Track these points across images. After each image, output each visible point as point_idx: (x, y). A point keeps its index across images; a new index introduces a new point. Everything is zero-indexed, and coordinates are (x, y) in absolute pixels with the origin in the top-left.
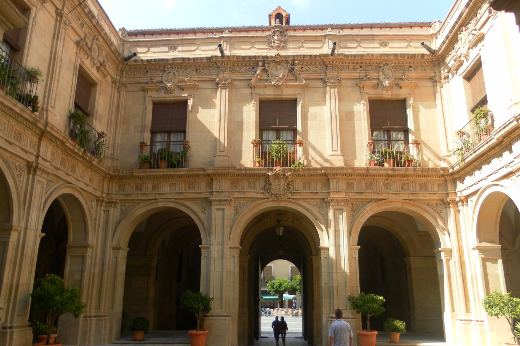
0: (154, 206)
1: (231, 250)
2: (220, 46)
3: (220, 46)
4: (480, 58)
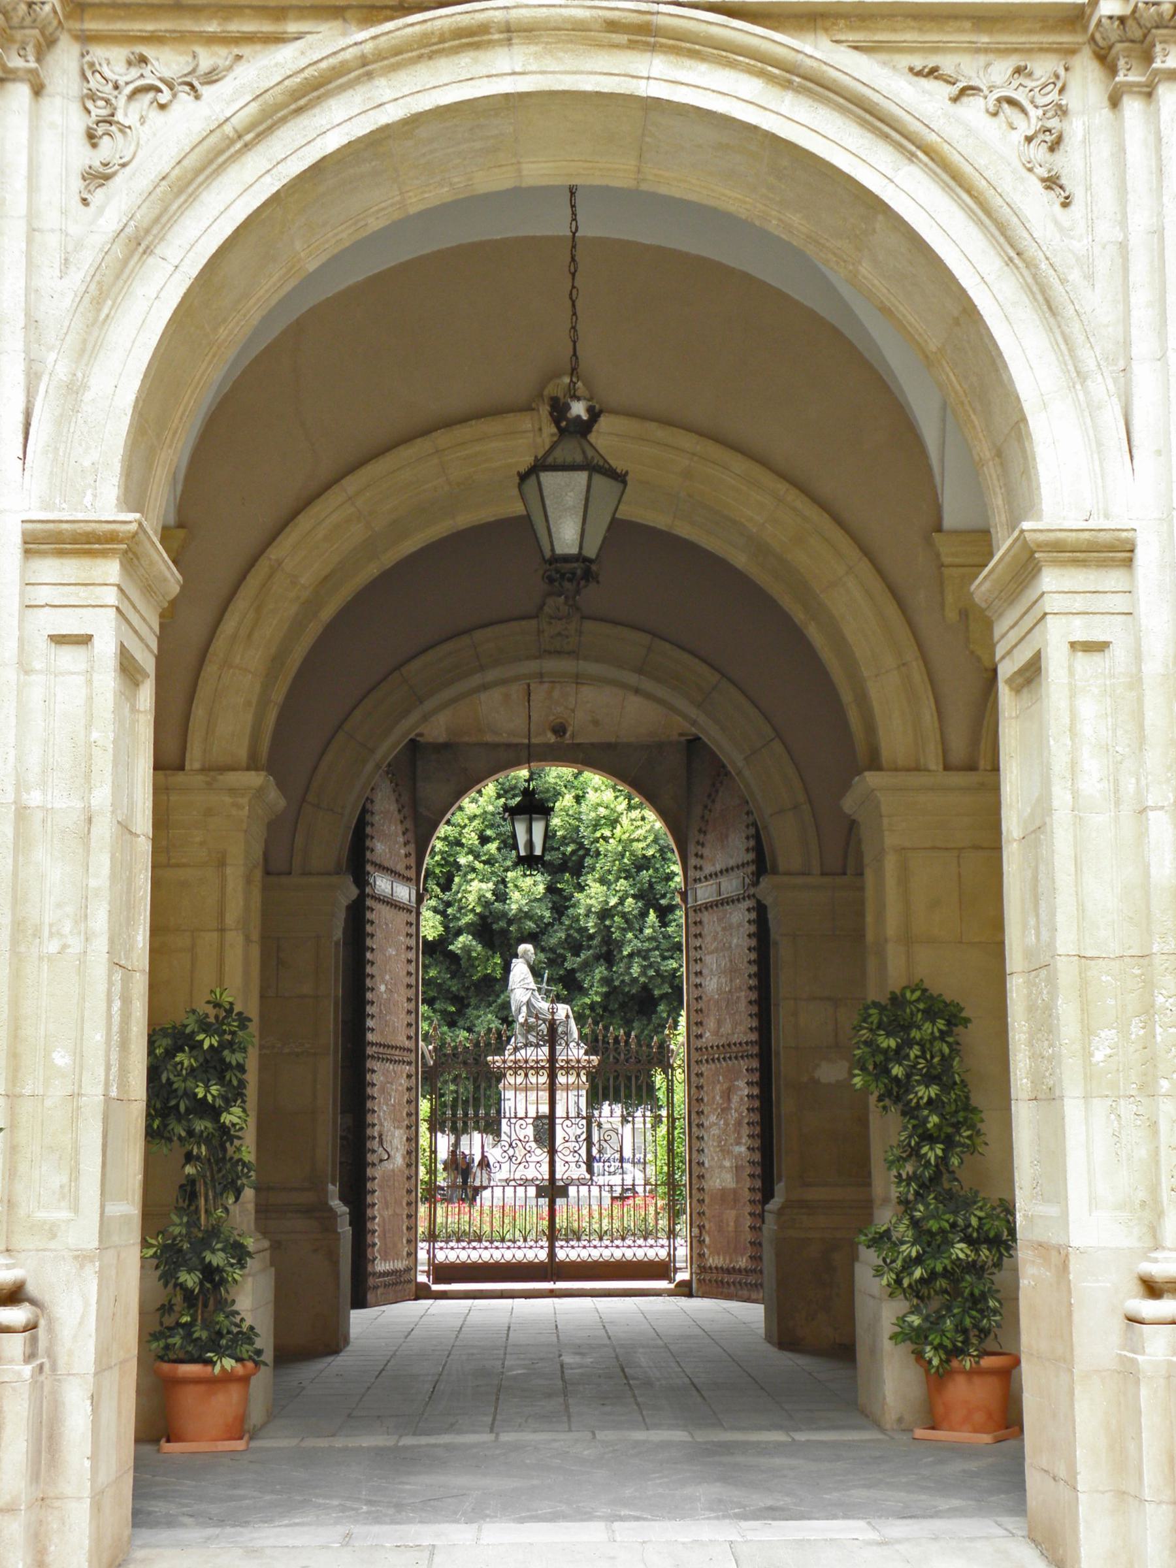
1: (49, 569)
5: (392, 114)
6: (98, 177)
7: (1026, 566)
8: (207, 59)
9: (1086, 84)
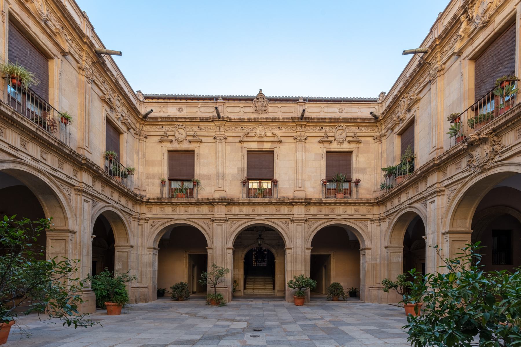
0: (172, 223)
2: (216, 108)
3: (216, 108)
4: (414, 118)
5: (12, 168)
9: (290, 222)
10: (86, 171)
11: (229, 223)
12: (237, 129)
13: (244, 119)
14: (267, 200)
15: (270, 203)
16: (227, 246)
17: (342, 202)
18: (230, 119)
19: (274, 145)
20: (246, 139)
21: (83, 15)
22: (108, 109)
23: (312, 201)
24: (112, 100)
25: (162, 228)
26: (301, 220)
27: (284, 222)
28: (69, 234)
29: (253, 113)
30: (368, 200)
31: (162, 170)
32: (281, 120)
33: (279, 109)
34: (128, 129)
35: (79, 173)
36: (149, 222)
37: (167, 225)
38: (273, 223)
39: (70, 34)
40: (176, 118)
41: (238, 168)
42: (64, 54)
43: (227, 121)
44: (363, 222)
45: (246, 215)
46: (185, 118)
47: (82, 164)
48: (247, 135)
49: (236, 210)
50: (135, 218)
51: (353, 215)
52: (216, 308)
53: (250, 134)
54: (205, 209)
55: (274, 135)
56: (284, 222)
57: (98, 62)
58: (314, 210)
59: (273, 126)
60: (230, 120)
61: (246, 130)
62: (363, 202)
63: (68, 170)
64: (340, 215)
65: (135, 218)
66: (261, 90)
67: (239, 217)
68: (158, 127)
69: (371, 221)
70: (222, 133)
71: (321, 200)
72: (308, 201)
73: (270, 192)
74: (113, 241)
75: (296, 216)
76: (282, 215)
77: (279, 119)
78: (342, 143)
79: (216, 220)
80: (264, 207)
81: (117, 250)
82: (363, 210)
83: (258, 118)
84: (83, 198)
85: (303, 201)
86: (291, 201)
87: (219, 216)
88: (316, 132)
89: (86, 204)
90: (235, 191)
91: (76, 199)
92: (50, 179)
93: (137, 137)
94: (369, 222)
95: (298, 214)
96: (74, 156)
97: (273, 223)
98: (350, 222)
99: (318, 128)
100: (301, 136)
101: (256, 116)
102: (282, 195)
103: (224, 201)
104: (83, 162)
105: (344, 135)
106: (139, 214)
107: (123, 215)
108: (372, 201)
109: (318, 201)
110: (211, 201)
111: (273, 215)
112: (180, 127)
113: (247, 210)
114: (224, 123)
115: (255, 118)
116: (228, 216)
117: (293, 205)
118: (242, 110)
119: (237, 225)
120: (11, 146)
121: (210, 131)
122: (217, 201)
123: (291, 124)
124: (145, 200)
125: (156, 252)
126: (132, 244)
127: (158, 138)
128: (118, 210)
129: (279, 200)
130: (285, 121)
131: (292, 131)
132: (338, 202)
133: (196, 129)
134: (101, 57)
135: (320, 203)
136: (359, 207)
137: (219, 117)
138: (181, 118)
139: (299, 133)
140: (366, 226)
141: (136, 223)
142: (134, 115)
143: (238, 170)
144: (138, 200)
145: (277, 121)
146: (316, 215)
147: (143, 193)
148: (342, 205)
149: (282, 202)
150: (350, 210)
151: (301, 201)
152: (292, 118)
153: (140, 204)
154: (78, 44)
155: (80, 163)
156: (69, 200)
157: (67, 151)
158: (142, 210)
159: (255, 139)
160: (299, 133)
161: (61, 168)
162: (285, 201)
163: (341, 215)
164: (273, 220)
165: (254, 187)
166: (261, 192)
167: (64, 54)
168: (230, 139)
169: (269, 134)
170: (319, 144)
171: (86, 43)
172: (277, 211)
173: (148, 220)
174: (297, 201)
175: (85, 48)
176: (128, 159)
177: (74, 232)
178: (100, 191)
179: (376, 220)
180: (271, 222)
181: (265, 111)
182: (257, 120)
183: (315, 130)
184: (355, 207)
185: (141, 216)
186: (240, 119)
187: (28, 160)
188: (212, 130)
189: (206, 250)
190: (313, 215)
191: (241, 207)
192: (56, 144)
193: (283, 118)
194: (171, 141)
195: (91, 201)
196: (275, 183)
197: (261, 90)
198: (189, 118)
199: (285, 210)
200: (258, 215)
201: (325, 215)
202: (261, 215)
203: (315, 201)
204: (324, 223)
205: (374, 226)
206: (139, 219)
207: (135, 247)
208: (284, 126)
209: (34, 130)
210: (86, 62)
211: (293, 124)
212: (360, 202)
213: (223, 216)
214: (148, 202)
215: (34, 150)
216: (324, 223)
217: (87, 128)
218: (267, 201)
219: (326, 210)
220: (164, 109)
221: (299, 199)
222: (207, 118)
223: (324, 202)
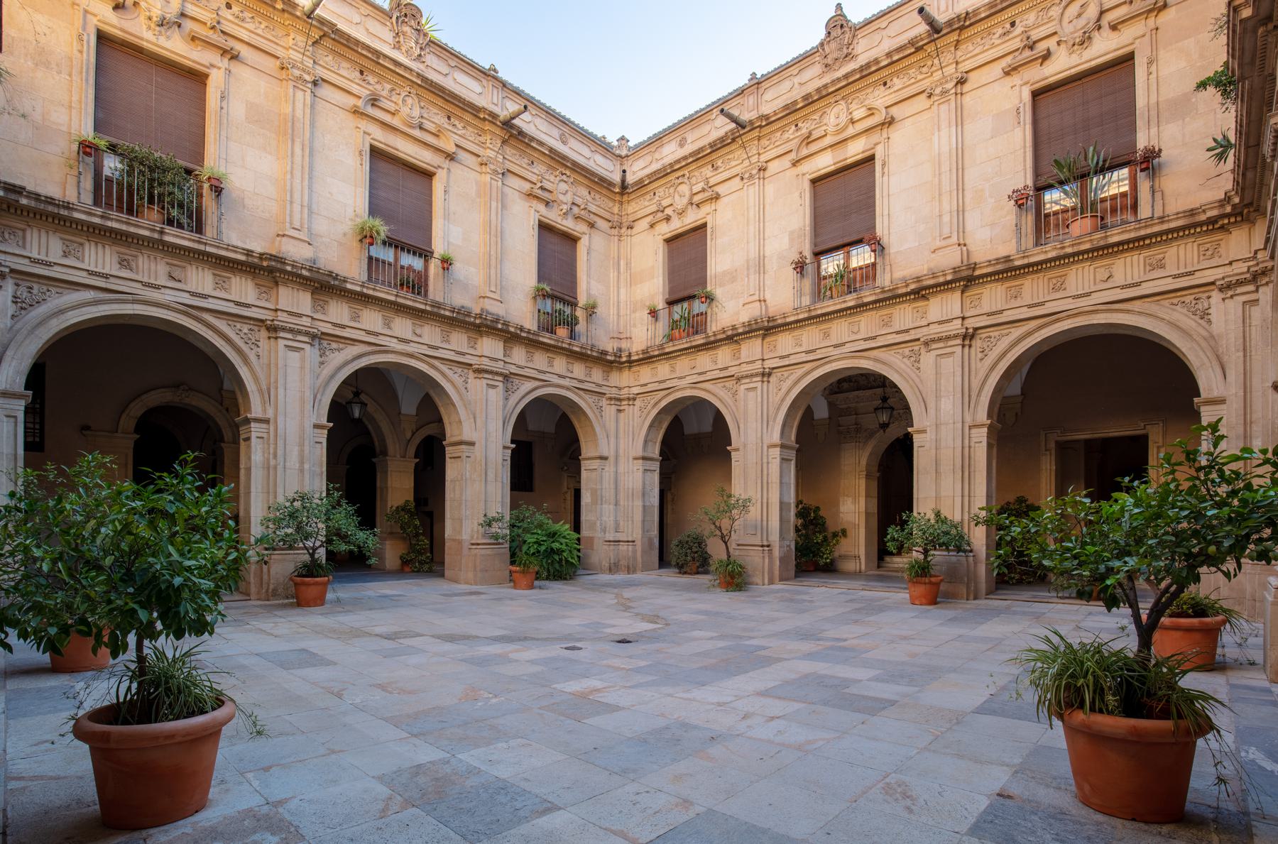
6: (322, 363)
7: (247, 421)
8: (341, 346)
9: (264, 333)
10: (488, 334)
11: (773, 379)
12: (786, 136)
13: (795, 102)
14: (850, 300)
15: (861, 307)
16: (767, 442)
17: (1087, 246)
18: (766, 117)
19: (875, 137)
20: (805, 152)
21: (488, 75)
22: (542, 208)
23: (977, 273)
24: (547, 185)
25: (655, 411)
26: (948, 338)
27: (907, 351)
28: (463, 447)
29: (820, 76)
30: (1192, 212)
31: (654, 288)
32: (883, 64)
33: (884, 33)
34: (592, 225)
35: (479, 342)
36: (638, 403)
37: (663, 403)
38: (876, 360)
39: (460, 119)
40: (671, 165)
41: (791, 233)
42: (451, 157)
43: (760, 127)
44: (1188, 299)
45: (807, 352)
46: (685, 158)
47: (479, 326)
48: (808, 140)
49: (338, 312)
50: (611, 399)
51: (1138, 284)
52: (557, 591)
53: (815, 135)
54: (243, 289)
55: (871, 112)
56: (907, 351)
57: (512, 135)
58: (992, 297)
59: (868, 86)
60: (767, 121)
61: (805, 127)
62: (1173, 225)
63: (459, 340)
64: (1088, 294)
65: (611, 399)
66: (839, 6)
67: (793, 360)
68: (648, 197)
69: (1220, 290)
70: (754, 159)
71: (1007, 259)
72: (964, 274)
73: (870, 272)
74: (578, 451)
75: (935, 329)
76: (898, 333)
77: (876, 61)
78: (1086, 40)
79: (284, 329)
80: (850, 320)
81: (585, 465)
82: (1183, 256)
83: (825, 86)
84: (485, 381)
85: (949, 278)
86: (913, 287)
87: (750, 367)
88: (993, 46)
89: (491, 391)
90: (784, 294)
91: (477, 386)
92: (428, 363)
93: (615, 232)
94: (1216, 296)
95: (940, 323)
96: (461, 317)
97: (876, 360)
98: (1128, 311)
99: (1000, 31)
100: (944, 80)
101: (827, 79)
102: (898, 274)
103: (754, 327)
104: (478, 321)
105: (568, 198)
106: (620, 389)
107: (580, 397)
108: (1214, 213)
109: (1000, 267)
110: (730, 333)
111: (874, 338)
112: (681, 180)
113: (810, 337)
114: (756, 133)
115: (818, 90)
116: (768, 364)
117: (924, 297)
118: (796, 80)
119: (789, 383)
120: (369, 333)
121: (733, 163)
122: (740, 330)
123: (913, 59)
124: (624, 359)
125: (656, 466)
126: (605, 454)
127: (644, 224)
128: (568, 389)
129: (883, 292)
130: (895, 58)
131: (920, 77)
132: (1069, 250)
133: (707, 171)
134: (513, 126)
135: (1008, 271)
136: (1162, 249)
137: (741, 125)
138: (678, 161)
139: (938, 75)
140: (1205, 315)
141: (614, 408)
142: (604, 191)
143: (791, 240)
144: (612, 362)
145: (873, 69)
146: (1001, 312)
147: (624, 345)
148: (1093, 259)
149: (891, 298)
150: (1127, 268)
151: (941, 280)
152: (911, 43)
153: (620, 369)
154: (475, 127)
155: (473, 324)
156: (464, 391)
157: (447, 313)
158: (625, 380)
159: (828, 141)
160: (938, 75)
161: (448, 342)
162: (900, 291)
163: (1090, 295)
164: (207, 317)
165: (861, 263)
166: (848, 281)
167: (451, 157)
168: (773, 167)
169: (858, 114)
170: (1008, 79)
171: (484, 119)
172: (886, 325)
173: (634, 399)
174: (931, 282)
175: (487, 127)
176: (593, 283)
177: (472, 444)
178: (523, 363)
179: (1240, 283)
180: (868, 358)
181: (849, 56)
182: (824, 93)
183: (988, 42)
184: (1146, 253)
185: (623, 392)
186: (786, 107)
187: (394, 345)
188: (735, 161)
189: (729, 453)
190: (989, 315)
191: (797, 333)
192: (428, 308)
193: (889, 55)
194: (668, 219)
195: (501, 384)
196: (878, 247)
197: (839, 6)
198: (691, 155)
199: (904, 316)
200: (836, 346)
201: (1030, 306)
202: (843, 344)
203: (990, 270)
204: (1030, 334)
205: (1234, 306)
206: (620, 400)
207: (612, 459)
208: (897, 74)
209: (393, 298)
210: (491, 147)
211: (920, 55)
212: (1156, 229)
213: (306, 321)
214: (631, 363)
215: (402, 326)
216: (1030, 334)
217: (497, 257)
218: (851, 304)
219: (1033, 289)
220: (657, 156)
221: (934, 276)
222: (722, 139)
223: (1017, 263)
